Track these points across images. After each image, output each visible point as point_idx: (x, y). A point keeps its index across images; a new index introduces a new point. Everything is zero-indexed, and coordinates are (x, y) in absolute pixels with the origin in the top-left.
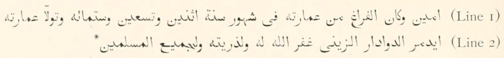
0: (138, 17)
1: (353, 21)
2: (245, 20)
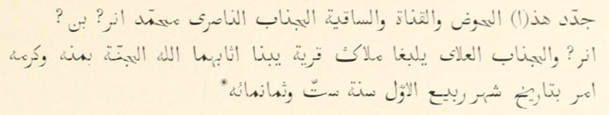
2: (485, 95)
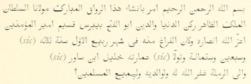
0: (233, 57)
1: (161, 43)
